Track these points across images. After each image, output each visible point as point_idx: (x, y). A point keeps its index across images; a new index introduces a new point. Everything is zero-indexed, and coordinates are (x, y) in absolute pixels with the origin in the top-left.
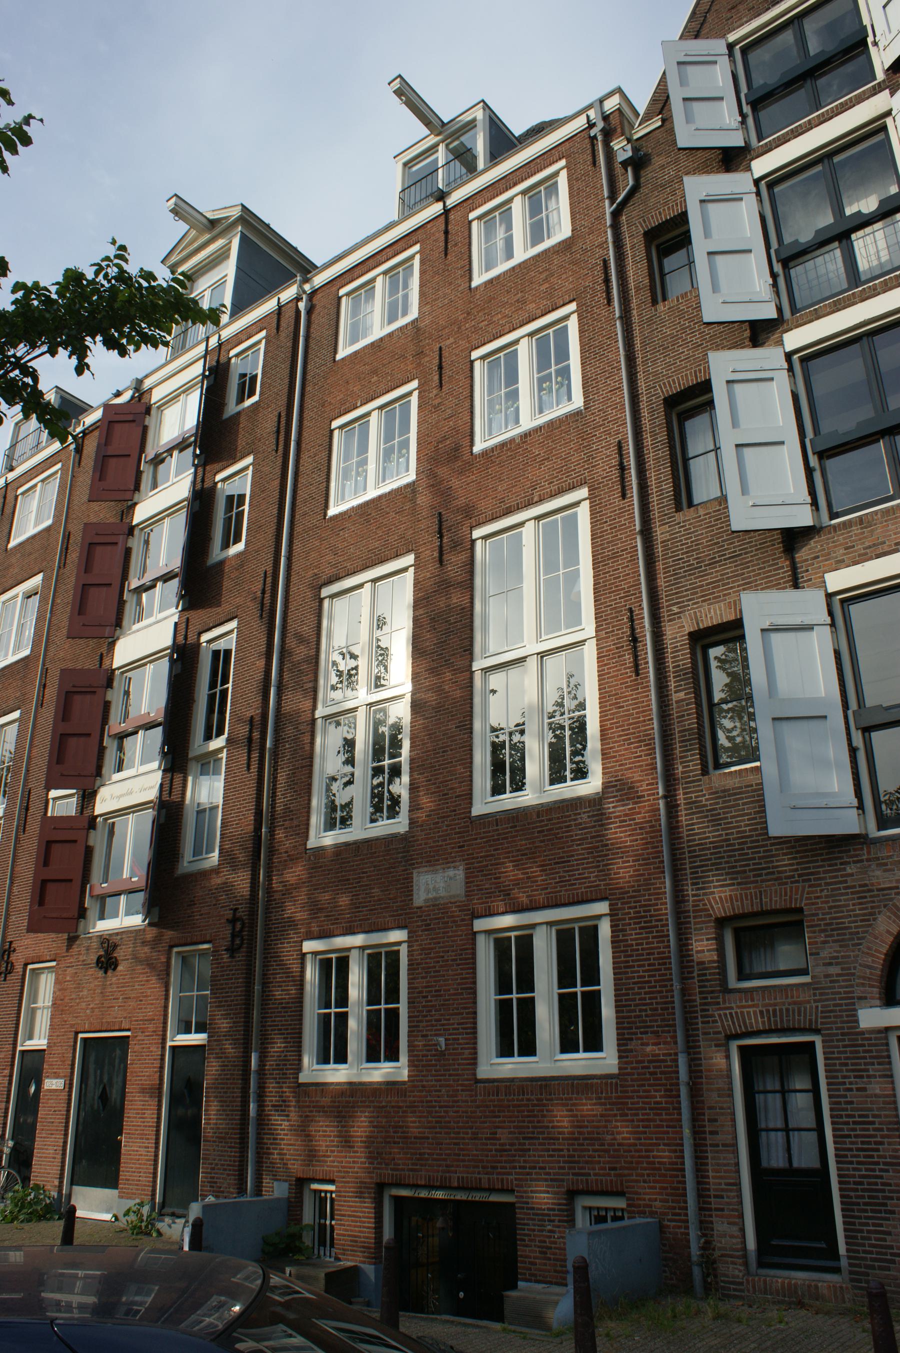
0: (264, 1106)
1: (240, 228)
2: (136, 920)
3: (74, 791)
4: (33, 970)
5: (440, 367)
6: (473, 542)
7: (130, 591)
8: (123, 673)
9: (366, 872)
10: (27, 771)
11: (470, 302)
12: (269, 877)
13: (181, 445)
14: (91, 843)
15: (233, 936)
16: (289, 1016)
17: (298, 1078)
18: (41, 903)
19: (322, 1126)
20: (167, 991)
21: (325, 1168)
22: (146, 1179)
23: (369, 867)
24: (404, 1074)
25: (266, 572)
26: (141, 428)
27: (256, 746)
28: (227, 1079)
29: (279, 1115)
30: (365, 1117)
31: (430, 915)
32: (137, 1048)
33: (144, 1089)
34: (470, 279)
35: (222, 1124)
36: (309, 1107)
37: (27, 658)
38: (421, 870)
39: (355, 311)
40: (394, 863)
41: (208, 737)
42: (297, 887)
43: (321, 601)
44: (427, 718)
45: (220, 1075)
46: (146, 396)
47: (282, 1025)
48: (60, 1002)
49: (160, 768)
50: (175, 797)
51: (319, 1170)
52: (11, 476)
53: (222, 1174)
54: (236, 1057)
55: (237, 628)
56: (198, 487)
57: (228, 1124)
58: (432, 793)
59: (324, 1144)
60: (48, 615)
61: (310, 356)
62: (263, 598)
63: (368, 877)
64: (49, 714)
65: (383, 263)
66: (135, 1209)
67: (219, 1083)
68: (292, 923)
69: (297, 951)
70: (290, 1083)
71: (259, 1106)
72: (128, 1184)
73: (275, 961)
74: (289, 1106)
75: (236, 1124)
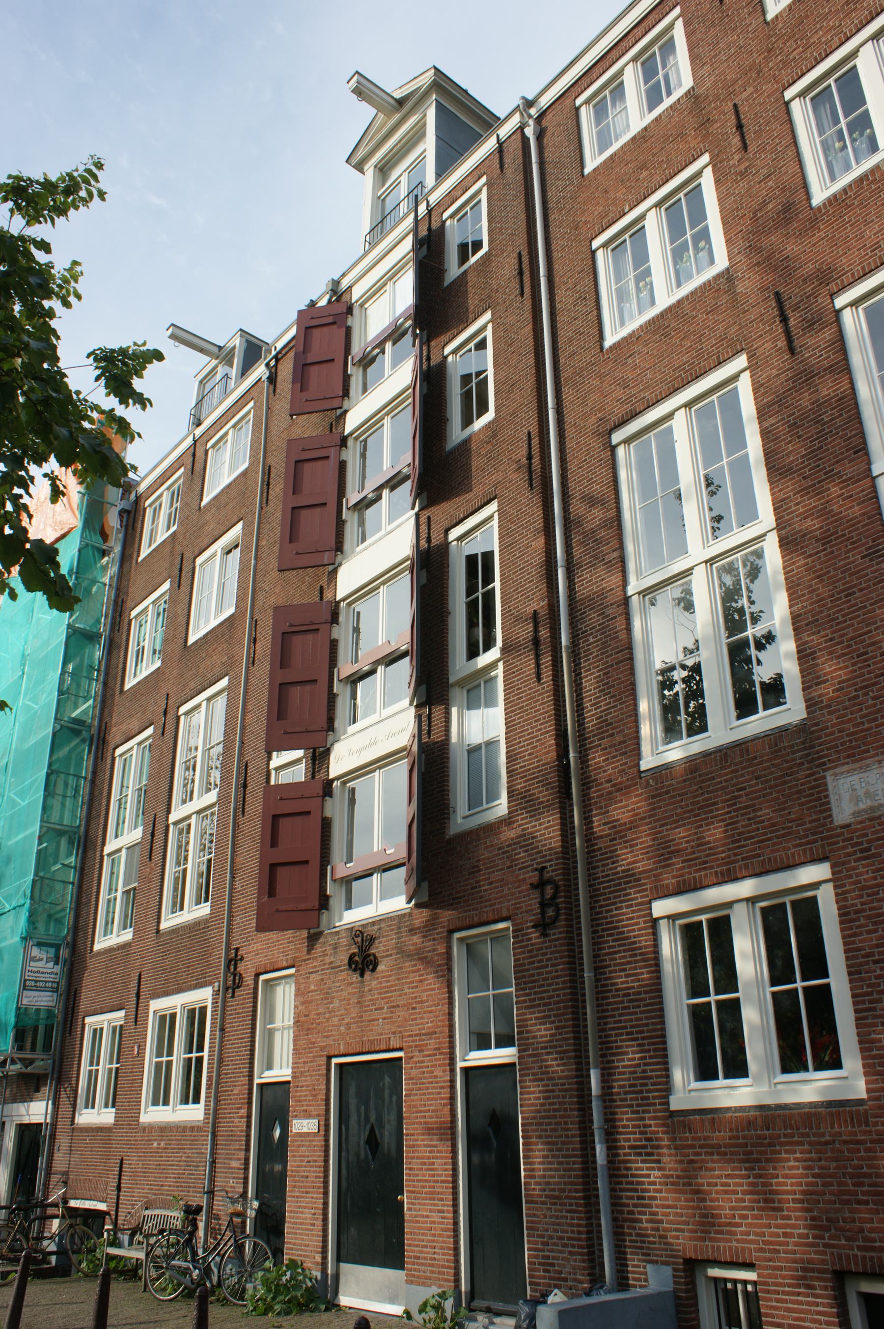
0: (616, 1148)
1: (434, 97)
2: (399, 903)
3: (300, 753)
4: (267, 981)
5: (740, 126)
6: (838, 312)
7: (349, 509)
8: (349, 604)
9: (744, 789)
10: (242, 742)
11: (770, 37)
12: (587, 819)
13: (395, 335)
14: (328, 813)
15: (543, 905)
16: (642, 1012)
17: (668, 1103)
18: (272, 893)
19: (720, 1177)
20: (450, 992)
21: (734, 1244)
22: (444, 1257)
23: (747, 781)
24: (859, 1088)
25: (529, 433)
26: (344, 330)
27: (545, 648)
28: (555, 1110)
29: (643, 1161)
30: (796, 1160)
31: (866, 835)
32: (414, 1073)
33: (429, 1129)
34: (764, 12)
35: (553, 1177)
36: (692, 1146)
37: (232, 616)
38: (838, 770)
39: (600, 112)
40: (790, 768)
41: (473, 653)
42: (632, 826)
43: (613, 449)
44: (810, 556)
45: (542, 1105)
46: (345, 298)
47: (632, 1027)
48: (304, 1019)
49: (411, 704)
50: (436, 737)
51: (725, 1247)
52: (199, 431)
53: (560, 1252)
54: (566, 1077)
55: (498, 510)
56: (425, 367)
57: (562, 1176)
58: (838, 657)
59: (727, 1205)
60: (253, 562)
61: (549, 183)
62: (530, 464)
63: (747, 795)
64: (263, 670)
65: (630, 48)
66: (432, 1302)
67: (542, 1117)
68: (631, 878)
69: (644, 916)
70: (655, 1111)
71: (609, 1148)
72: (418, 1264)
73: (609, 935)
74: (658, 1147)
75: (576, 1176)
